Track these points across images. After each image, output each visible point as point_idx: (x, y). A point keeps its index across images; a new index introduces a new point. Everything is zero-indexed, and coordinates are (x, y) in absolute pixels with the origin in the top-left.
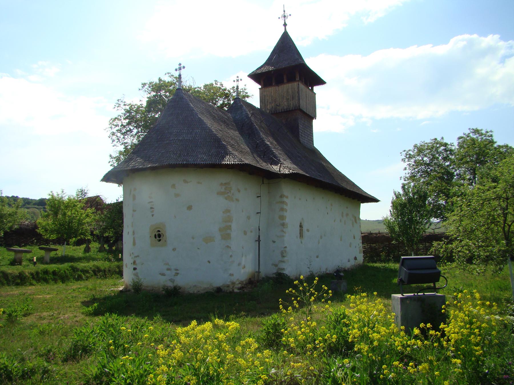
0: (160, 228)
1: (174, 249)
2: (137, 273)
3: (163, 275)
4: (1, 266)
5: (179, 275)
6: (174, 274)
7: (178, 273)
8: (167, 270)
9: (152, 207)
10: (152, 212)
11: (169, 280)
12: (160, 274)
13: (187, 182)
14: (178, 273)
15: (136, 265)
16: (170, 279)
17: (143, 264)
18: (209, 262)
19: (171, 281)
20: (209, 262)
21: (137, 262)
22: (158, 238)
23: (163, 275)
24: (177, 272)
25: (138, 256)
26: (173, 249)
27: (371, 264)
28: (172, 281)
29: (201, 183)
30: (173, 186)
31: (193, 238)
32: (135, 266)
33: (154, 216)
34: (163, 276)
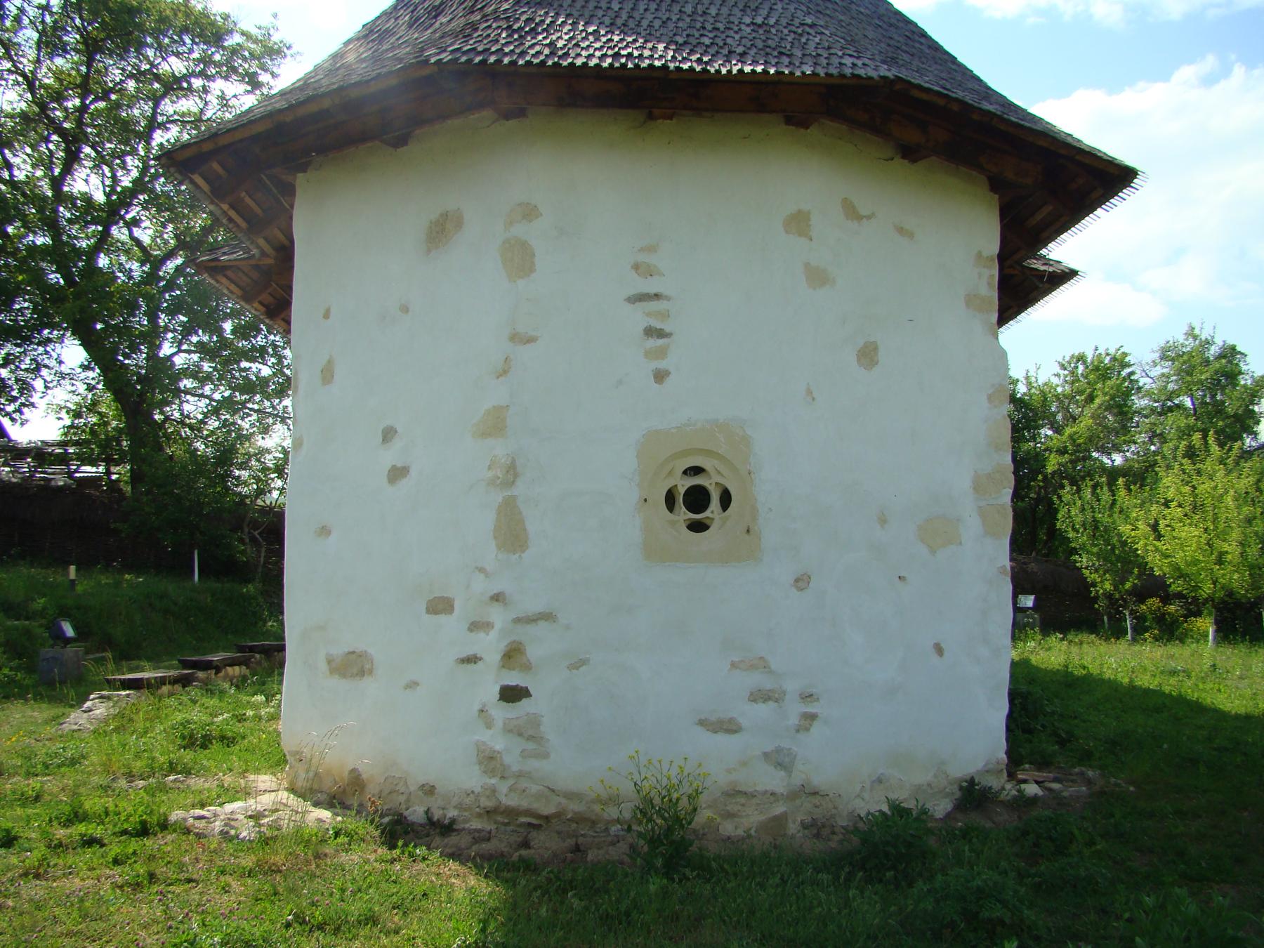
0: (708, 453)
1: (801, 582)
2: (535, 721)
3: (729, 727)
4: (2, 31)
5: (816, 728)
6: (794, 720)
7: (812, 717)
8: (755, 701)
9: (658, 325)
10: (661, 353)
11: (766, 755)
12: (702, 723)
13: (860, 218)
14: (812, 717)
15: (527, 667)
16: (769, 749)
17: (583, 662)
18: (939, 650)
19: (780, 765)
20: (939, 650)
21: (534, 652)
22: (684, 514)
23: (729, 727)
24: (810, 709)
25: (547, 617)
26: (797, 580)
27: (1106, 625)
28: (780, 760)
29: (911, 235)
30: (799, 223)
31: (883, 521)
32: (513, 679)
33: (669, 381)
34: (721, 738)
